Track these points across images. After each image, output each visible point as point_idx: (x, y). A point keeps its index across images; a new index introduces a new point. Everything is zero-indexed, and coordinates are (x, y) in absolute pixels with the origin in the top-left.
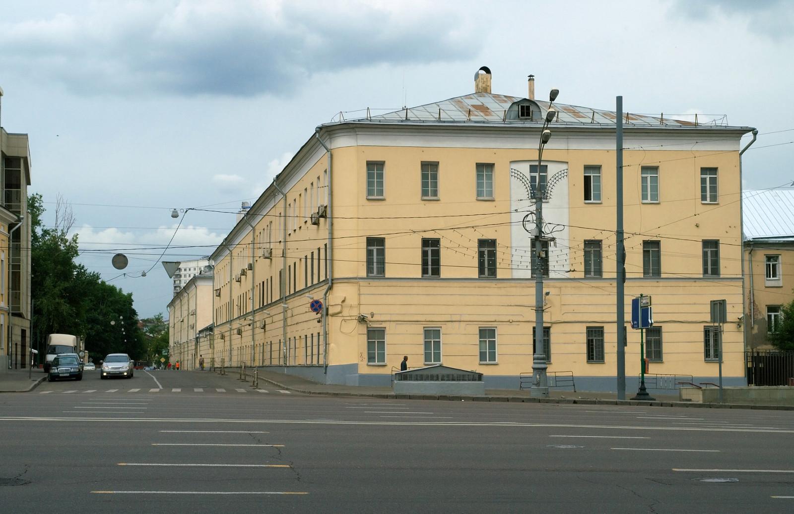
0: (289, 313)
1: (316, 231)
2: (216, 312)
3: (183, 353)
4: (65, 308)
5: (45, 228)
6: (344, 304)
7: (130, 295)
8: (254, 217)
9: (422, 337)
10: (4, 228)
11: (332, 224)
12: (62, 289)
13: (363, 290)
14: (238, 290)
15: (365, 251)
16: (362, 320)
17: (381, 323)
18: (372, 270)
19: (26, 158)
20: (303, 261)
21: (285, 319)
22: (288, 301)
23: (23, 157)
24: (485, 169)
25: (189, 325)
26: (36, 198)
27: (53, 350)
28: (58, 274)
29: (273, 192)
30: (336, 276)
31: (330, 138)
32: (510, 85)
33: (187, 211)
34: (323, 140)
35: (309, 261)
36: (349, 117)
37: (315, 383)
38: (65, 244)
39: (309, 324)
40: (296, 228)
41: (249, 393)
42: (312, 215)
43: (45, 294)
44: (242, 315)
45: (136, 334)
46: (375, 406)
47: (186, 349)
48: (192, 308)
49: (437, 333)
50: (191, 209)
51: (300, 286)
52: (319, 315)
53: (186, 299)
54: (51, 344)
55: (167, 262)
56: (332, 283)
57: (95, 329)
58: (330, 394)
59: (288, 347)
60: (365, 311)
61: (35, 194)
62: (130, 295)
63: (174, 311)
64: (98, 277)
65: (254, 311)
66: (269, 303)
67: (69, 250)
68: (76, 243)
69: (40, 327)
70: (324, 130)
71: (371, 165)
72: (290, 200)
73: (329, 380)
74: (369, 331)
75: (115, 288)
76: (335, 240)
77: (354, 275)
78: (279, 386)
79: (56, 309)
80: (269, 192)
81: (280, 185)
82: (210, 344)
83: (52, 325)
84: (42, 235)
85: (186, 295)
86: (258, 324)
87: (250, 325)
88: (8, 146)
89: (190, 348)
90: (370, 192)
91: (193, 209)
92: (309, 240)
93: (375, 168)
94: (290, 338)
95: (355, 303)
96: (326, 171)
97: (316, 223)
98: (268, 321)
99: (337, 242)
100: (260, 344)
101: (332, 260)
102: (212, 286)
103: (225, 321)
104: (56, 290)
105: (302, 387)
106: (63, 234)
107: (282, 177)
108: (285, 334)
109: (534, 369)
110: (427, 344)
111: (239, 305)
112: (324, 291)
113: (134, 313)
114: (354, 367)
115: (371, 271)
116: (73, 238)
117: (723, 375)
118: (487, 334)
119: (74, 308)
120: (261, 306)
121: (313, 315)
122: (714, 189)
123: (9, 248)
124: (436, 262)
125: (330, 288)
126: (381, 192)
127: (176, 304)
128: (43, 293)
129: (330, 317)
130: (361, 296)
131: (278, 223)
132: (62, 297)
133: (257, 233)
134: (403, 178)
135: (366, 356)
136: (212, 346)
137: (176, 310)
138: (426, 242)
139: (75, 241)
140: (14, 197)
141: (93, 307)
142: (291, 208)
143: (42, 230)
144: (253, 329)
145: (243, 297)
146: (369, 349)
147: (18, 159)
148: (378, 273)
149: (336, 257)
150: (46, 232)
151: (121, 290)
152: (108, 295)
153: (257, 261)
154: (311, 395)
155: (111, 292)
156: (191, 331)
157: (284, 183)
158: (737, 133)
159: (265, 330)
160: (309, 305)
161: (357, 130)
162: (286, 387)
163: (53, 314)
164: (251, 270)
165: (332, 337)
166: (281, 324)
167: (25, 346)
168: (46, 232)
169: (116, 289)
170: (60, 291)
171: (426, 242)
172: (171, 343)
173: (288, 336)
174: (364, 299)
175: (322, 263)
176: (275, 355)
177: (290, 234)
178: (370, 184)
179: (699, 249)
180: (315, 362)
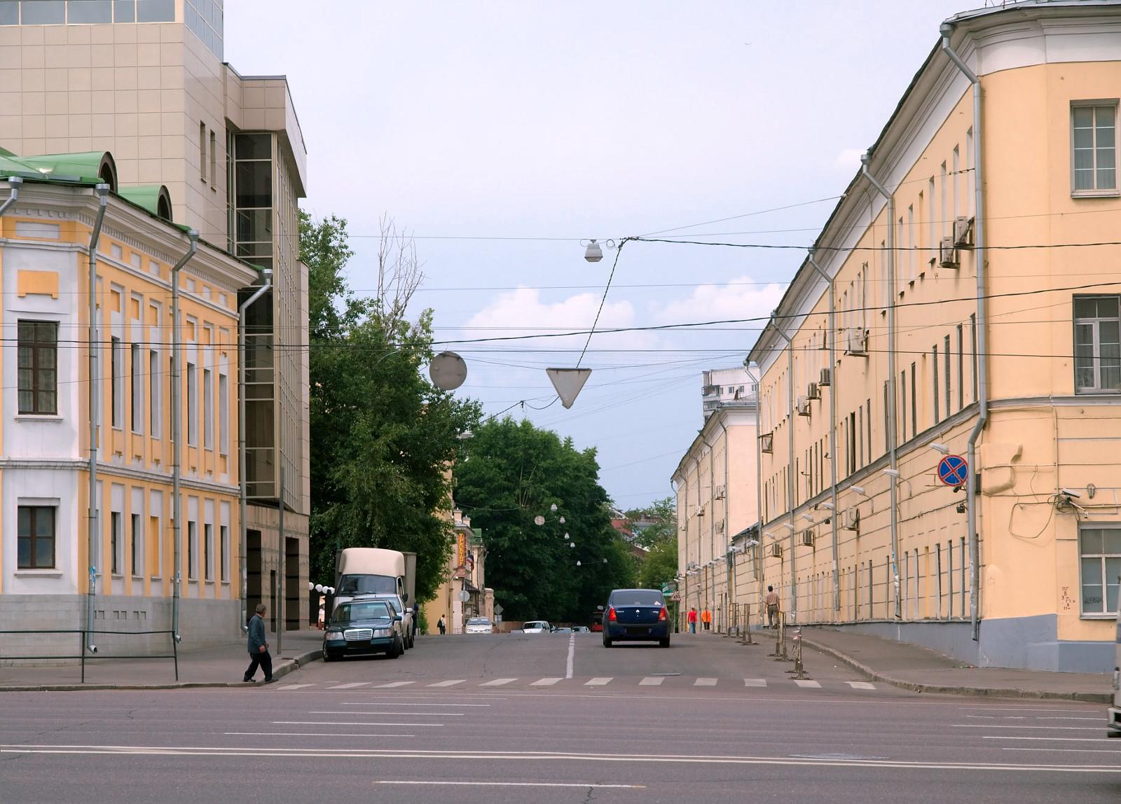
0: (904, 491)
1: (953, 281)
2: (764, 492)
3: (704, 593)
4: (401, 485)
5: (353, 298)
6: (1018, 464)
7: (591, 454)
8: (831, 254)
10: (226, 301)
11: (986, 265)
12: (394, 442)
13: (1066, 429)
15: (1069, 327)
16: (1066, 503)
17: (1114, 511)
18: (1089, 378)
19: (284, 131)
20: (930, 357)
21: (896, 507)
22: (902, 461)
23: (275, 132)
25: (714, 524)
26: (331, 227)
27: (353, 585)
28: (384, 404)
29: (866, 190)
30: (998, 394)
31: (979, 49)
33: (623, 243)
34: (961, 57)
35: (941, 359)
37: (953, 665)
38: (403, 334)
39: (936, 515)
40: (915, 276)
41: (771, 688)
42: (941, 244)
43: (353, 456)
44: (814, 495)
45: (607, 547)
46: (1046, 723)
47: (710, 583)
48: (719, 482)
50: (631, 239)
51: (926, 422)
52: (961, 495)
53: (708, 458)
54: (344, 573)
55: (558, 370)
56: (989, 413)
57: (511, 533)
58: (968, 691)
59: (904, 577)
60: (1073, 482)
61: (329, 219)
62: (591, 454)
63: (687, 490)
64: (476, 411)
65: (836, 486)
66: (864, 466)
67: (409, 346)
68: (428, 331)
69: (344, 533)
70: (961, 30)
72: (902, 210)
73: (987, 654)
74: (1082, 532)
75: (554, 436)
76: (994, 302)
77: (1044, 392)
78: (862, 672)
79: (380, 490)
80: (857, 191)
81: (880, 174)
82: (756, 569)
83: (370, 526)
84: (348, 314)
85: (707, 449)
86: (846, 520)
87: (828, 522)
88: (242, 108)
89: (717, 580)
90: (1081, 180)
91: (637, 239)
92: (937, 308)
94: (907, 553)
95: (1046, 460)
96: (970, 132)
98: (865, 510)
99: (997, 305)
100: (823, 573)
101: (987, 355)
102: (755, 428)
103: (783, 513)
104: (380, 445)
105: (915, 675)
106: (399, 309)
107: (880, 155)
108: (896, 542)
111: (809, 473)
112: (970, 433)
113: (600, 495)
114: (1045, 624)
115: (1086, 380)
116: (421, 321)
119: (421, 486)
120: (850, 474)
121: (948, 494)
123: (239, 345)
125: (985, 425)
127: (689, 473)
128: (349, 451)
129: (984, 498)
130: (1060, 442)
131: (878, 261)
132: (393, 457)
133: (840, 294)
135: (1076, 595)
136: (759, 575)
137: (689, 488)
139: (426, 327)
140: (259, 225)
141: (506, 483)
142: (904, 226)
143: (348, 301)
144: (836, 530)
145: (816, 452)
146: (1085, 577)
147: (265, 136)
149: (996, 348)
150: (356, 308)
151: (569, 441)
152: (538, 455)
153: (839, 361)
154: (922, 694)
155: (546, 447)
156: (719, 539)
157: (889, 167)
159: (858, 533)
160: (935, 471)
161: (1044, 23)
162: (874, 673)
163: (371, 500)
164: (828, 385)
165: (990, 549)
166: (886, 518)
167: (297, 577)
168: (356, 308)
169: (557, 440)
170: (388, 446)
172: (682, 570)
174: (1069, 452)
175: (968, 360)
176: (879, 593)
177: (902, 294)
178: (1080, 159)
180: (957, 613)
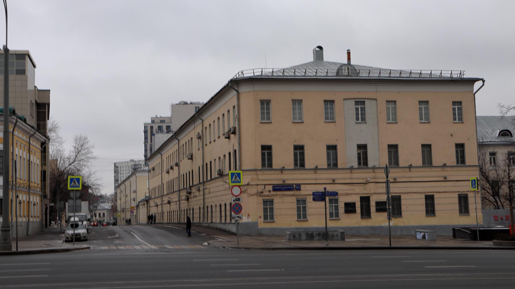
0: (207, 191)
9: (296, 204)
14: (167, 178)
24: (329, 103)
32: (334, 56)
36: (248, 74)
71: (262, 102)
72: (206, 124)
92: (219, 148)
93: (265, 104)
97: (228, 138)
109: (2, 231)
110: (299, 208)
114: (256, 224)
117: (328, 226)
118: (430, 200)
122: (460, 114)
124: (303, 160)
126: (269, 118)
134: (346, 110)
138: (329, 147)
146: (264, 212)
148: (268, 166)
158: (472, 81)
166: (202, 197)
171: (329, 147)
173: (206, 205)
179: (453, 150)
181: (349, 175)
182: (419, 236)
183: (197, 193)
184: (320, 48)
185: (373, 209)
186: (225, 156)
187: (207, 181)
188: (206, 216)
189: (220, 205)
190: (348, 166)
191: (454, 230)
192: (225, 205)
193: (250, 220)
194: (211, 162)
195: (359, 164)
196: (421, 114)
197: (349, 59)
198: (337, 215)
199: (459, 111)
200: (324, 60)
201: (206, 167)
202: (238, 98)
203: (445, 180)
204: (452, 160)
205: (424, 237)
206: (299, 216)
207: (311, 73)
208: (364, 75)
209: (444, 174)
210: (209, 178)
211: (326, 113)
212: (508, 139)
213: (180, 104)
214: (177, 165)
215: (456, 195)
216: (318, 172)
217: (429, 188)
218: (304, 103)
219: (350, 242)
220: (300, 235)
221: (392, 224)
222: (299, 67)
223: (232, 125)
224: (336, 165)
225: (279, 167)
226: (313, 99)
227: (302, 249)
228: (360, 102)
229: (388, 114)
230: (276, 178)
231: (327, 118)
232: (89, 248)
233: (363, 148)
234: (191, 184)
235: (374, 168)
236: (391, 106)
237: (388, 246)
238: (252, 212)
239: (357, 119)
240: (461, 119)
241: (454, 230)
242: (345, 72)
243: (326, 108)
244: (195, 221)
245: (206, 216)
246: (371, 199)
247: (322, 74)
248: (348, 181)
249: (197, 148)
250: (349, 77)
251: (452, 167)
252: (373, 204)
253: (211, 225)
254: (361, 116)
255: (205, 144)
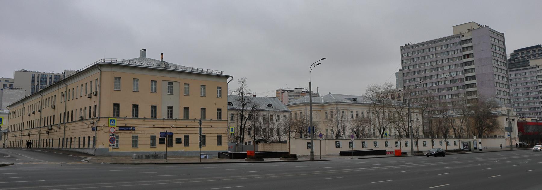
0: (67, 129)
14: (26, 119)
36: (107, 61)
49: (137, 137)
110: (133, 141)
114: (108, 149)
122: (220, 93)
124: (172, 114)
125: (99, 120)
134: (162, 86)
138: (152, 107)
158: (227, 77)
171: (152, 107)
179: (216, 111)
181: (162, 123)
182: (203, 157)
183: (58, 130)
184: (145, 50)
185: (174, 142)
186: (86, 108)
187: (68, 122)
188: (65, 143)
189: (80, 138)
190: (162, 118)
191: (219, 153)
192: (84, 138)
193: (103, 147)
194: (72, 111)
195: (168, 117)
196: (201, 92)
197: (162, 58)
198: (155, 145)
199: (220, 91)
200: (147, 57)
201: (66, 115)
202: (101, 75)
203: (211, 127)
204: (215, 117)
205: (206, 157)
206: (133, 145)
207: (138, 64)
208: (173, 68)
209: (211, 124)
210: (70, 121)
211: (152, 88)
212: (232, 107)
213: (21, 71)
214: (40, 111)
215: (216, 135)
216: (146, 120)
217: (220, 132)
218: (140, 81)
219: (170, 160)
220: (142, 156)
221: (202, 150)
222: (132, 60)
223: (94, 90)
224: (155, 117)
225: (193, 119)
226: (145, 78)
227: (155, 164)
228: (117, 79)
229: (185, 91)
230: (119, 123)
231: (152, 90)
232: (13, 164)
233: (170, 108)
234: (52, 124)
235: (176, 119)
236: (187, 86)
237: (199, 162)
238: (103, 142)
239: (168, 92)
240: (220, 96)
241: (219, 153)
242: (163, 66)
243: (152, 85)
244: (54, 147)
245: (65, 143)
246: (174, 136)
247: (144, 64)
248: (162, 126)
249: (60, 101)
250: (164, 69)
251: (215, 120)
252: (174, 139)
253: (70, 150)
254: (170, 91)
255: (68, 99)
